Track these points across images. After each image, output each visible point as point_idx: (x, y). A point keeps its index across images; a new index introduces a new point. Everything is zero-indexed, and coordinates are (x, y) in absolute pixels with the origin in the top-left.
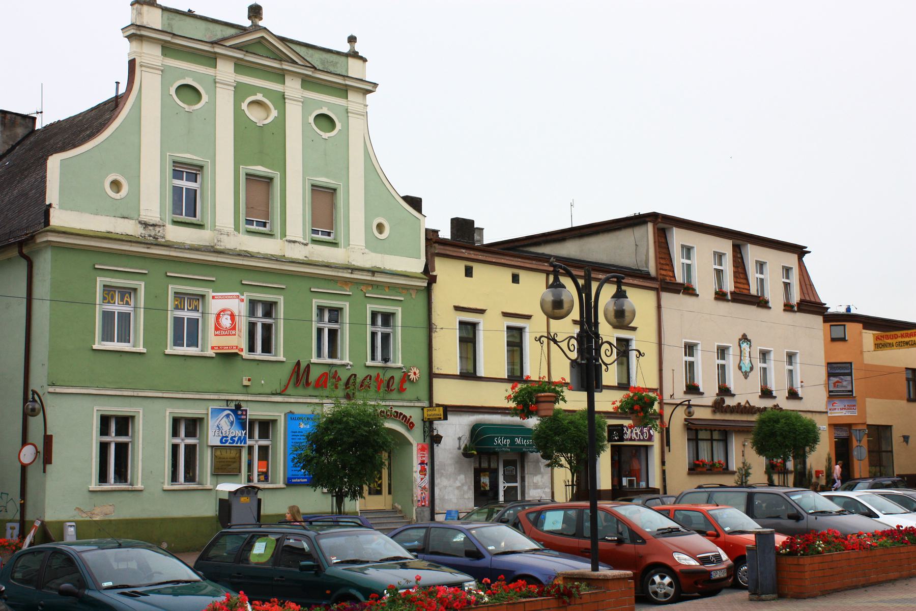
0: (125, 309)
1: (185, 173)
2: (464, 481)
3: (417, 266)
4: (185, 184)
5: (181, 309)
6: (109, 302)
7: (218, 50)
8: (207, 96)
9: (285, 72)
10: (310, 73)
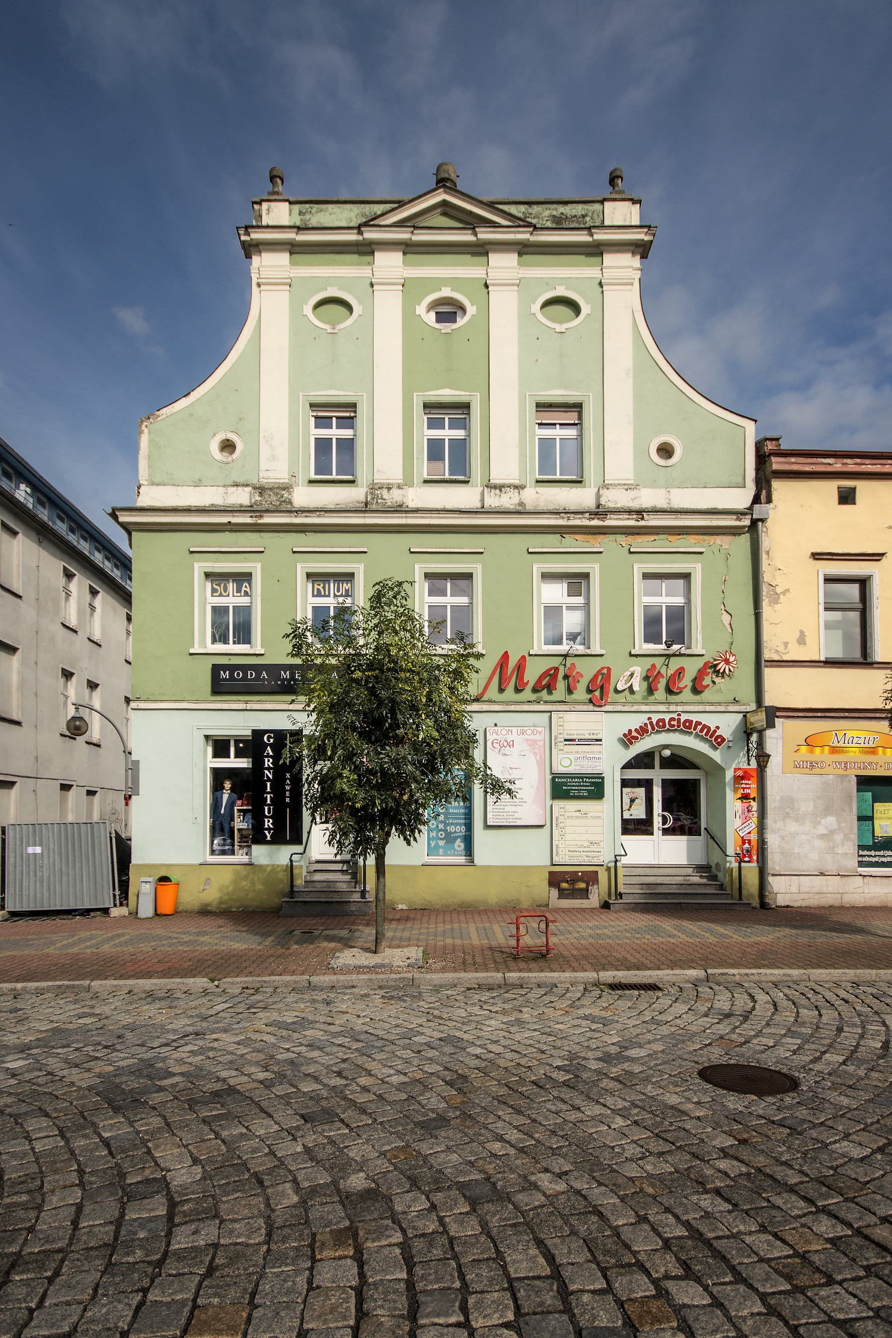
0: (244, 601)
1: (334, 419)
2: (835, 826)
3: (741, 498)
4: (335, 433)
5: (325, 596)
6: (221, 595)
7: (370, 235)
8: (361, 307)
9: (487, 247)
10: (526, 236)
